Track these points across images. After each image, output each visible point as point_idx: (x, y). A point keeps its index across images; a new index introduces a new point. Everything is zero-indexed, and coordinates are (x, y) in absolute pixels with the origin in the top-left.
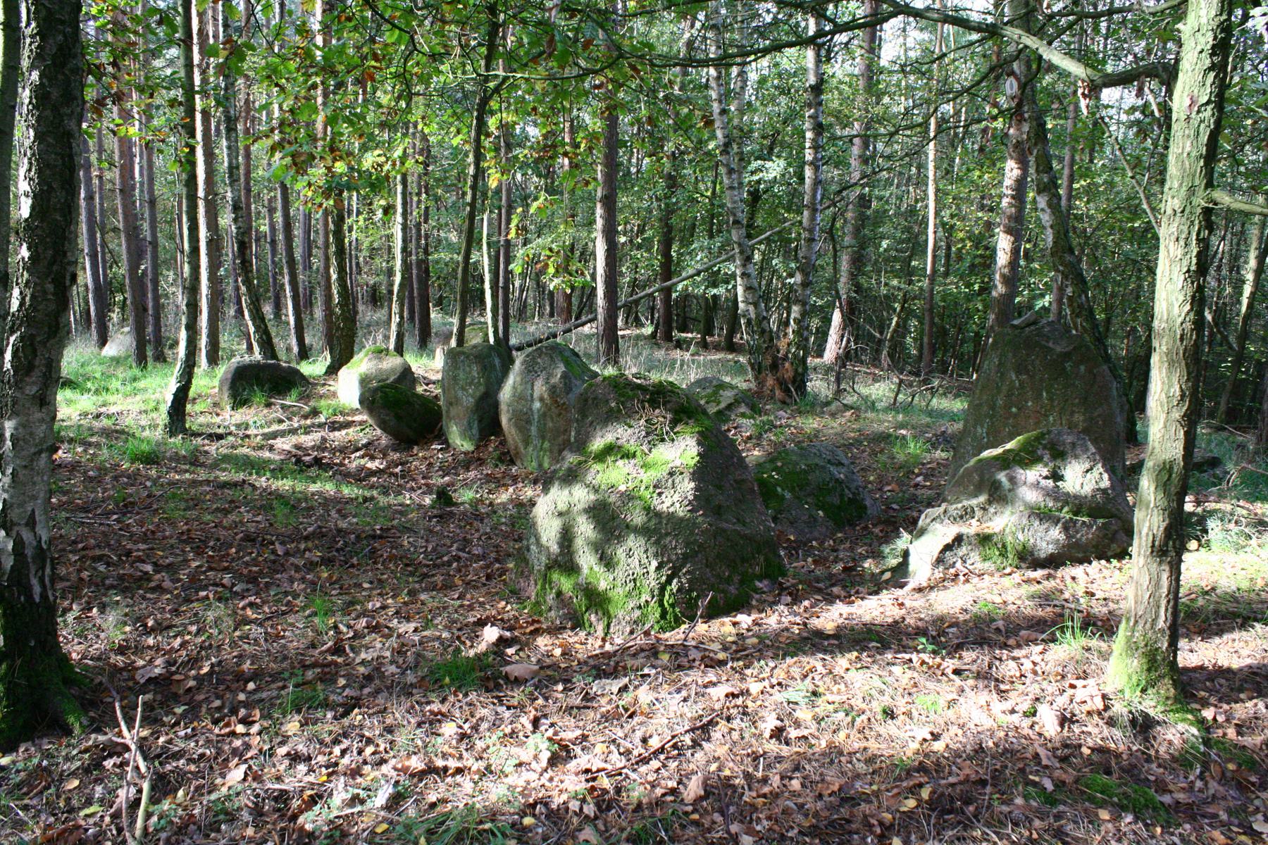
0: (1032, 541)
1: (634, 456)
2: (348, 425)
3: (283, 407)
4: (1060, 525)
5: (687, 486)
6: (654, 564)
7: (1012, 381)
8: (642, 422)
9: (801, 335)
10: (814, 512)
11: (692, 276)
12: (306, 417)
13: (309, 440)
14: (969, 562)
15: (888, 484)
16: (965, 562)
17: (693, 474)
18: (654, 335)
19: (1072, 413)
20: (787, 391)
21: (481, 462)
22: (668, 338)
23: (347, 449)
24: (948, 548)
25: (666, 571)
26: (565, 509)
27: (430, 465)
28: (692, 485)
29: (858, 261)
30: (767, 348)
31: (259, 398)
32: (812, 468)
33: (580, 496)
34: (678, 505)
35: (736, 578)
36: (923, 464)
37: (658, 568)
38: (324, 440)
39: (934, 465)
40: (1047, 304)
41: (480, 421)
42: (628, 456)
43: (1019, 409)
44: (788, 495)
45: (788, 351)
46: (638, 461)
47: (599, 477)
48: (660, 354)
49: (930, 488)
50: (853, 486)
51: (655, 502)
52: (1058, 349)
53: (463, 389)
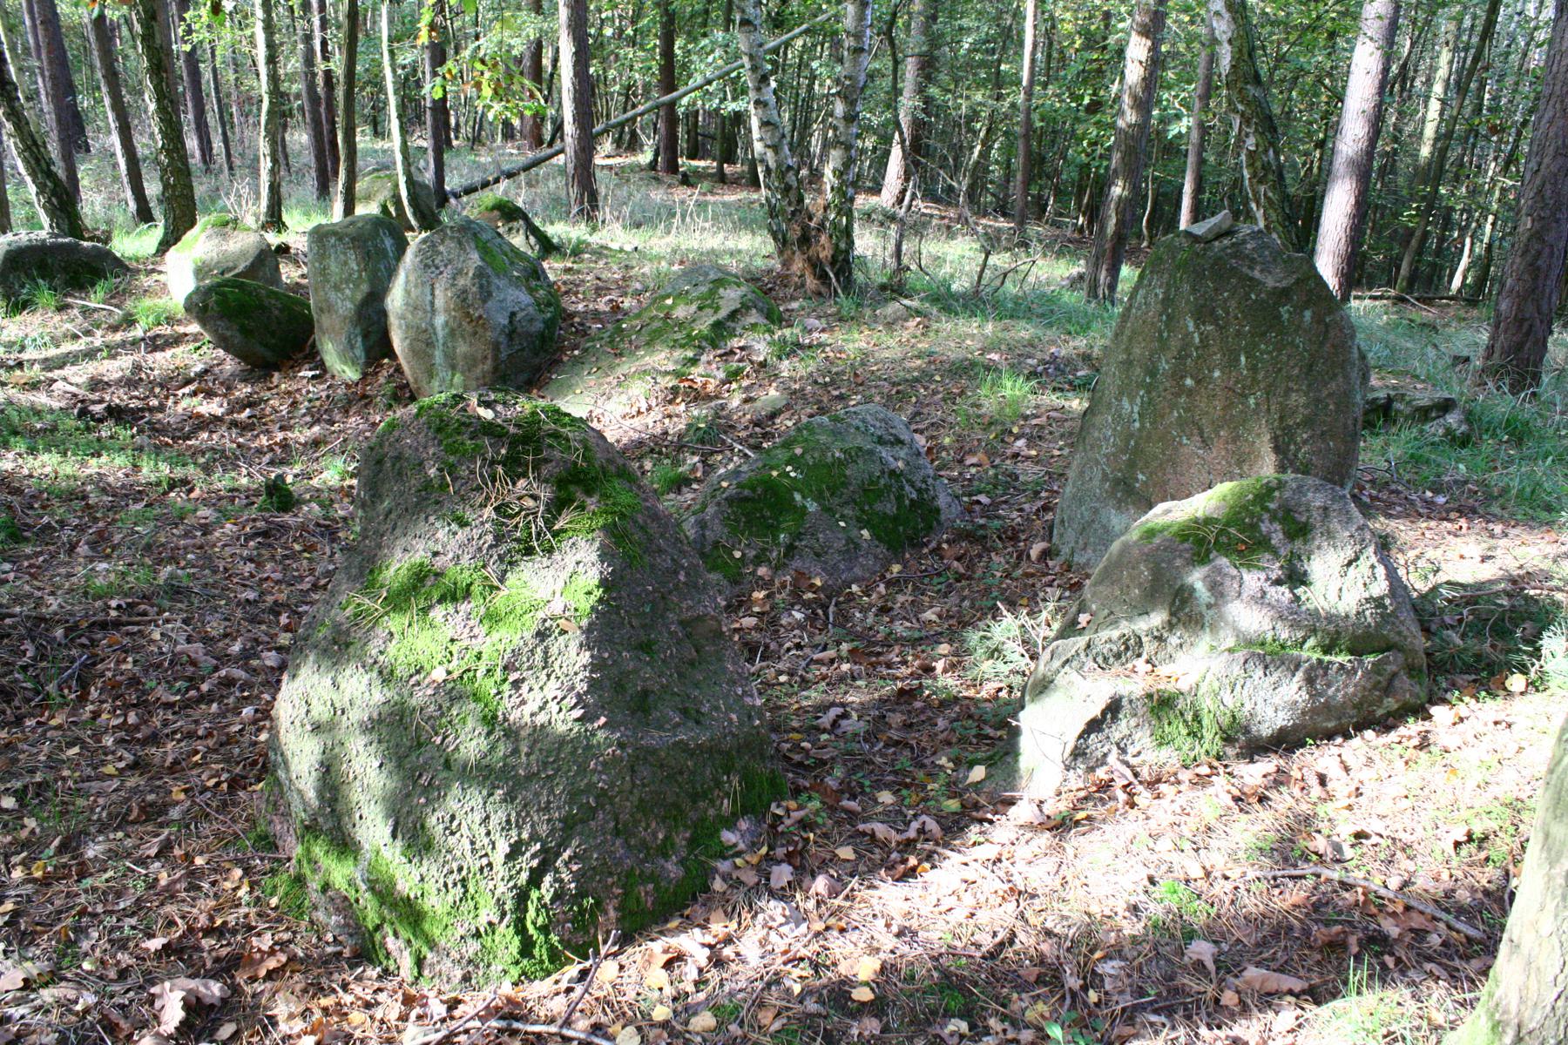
0: (1248, 707)
1: (467, 594)
2: (177, 340)
3: (86, 312)
4: (1300, 675)
5: (573, 658)
6: (503, 847)
7: (1188, 334)
8: (488, 512)
9: (844, 194)
10: (854, 533)
11: (700, 87)
12: (114, 329)
13: (113, 369)
14: (1131, 750)
15: (971, 452)
16: (1124, 751)
17: (588, 631)
18: (653, 165)
19: (1288, 391)
20: (823, 277)
21: (366, 400)
22: (672, 167)
23: (171, 383)
24: (1094, 726)
25: (527, 862)
26: (326, 717)
27: (294, 404)
28: (586, 657)
29: (928, 66)
30: (793, 213)
31: (46, 297)
32: (853, 455)
33: (357, 691)
34: (553, 706)
35: (681, 839)
36: (1026, 418)
37: (515, 852)
38: (137, 368)
39: (1042, 421)
40: (1184, 130)
41: (365, 336)
42: (456, 595)
43: (1198, 382)
44: (812, 506)
45: (825, 218)
46: (474, 606)
47: (392, 649)
48: (657, 195)
49: (1036, 460)
50: (917, 478)
51: (507, 704)
52: (1270, 282)
53: (337, 288)
